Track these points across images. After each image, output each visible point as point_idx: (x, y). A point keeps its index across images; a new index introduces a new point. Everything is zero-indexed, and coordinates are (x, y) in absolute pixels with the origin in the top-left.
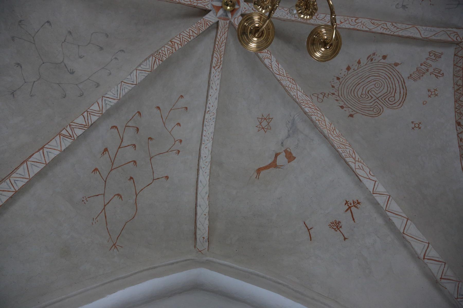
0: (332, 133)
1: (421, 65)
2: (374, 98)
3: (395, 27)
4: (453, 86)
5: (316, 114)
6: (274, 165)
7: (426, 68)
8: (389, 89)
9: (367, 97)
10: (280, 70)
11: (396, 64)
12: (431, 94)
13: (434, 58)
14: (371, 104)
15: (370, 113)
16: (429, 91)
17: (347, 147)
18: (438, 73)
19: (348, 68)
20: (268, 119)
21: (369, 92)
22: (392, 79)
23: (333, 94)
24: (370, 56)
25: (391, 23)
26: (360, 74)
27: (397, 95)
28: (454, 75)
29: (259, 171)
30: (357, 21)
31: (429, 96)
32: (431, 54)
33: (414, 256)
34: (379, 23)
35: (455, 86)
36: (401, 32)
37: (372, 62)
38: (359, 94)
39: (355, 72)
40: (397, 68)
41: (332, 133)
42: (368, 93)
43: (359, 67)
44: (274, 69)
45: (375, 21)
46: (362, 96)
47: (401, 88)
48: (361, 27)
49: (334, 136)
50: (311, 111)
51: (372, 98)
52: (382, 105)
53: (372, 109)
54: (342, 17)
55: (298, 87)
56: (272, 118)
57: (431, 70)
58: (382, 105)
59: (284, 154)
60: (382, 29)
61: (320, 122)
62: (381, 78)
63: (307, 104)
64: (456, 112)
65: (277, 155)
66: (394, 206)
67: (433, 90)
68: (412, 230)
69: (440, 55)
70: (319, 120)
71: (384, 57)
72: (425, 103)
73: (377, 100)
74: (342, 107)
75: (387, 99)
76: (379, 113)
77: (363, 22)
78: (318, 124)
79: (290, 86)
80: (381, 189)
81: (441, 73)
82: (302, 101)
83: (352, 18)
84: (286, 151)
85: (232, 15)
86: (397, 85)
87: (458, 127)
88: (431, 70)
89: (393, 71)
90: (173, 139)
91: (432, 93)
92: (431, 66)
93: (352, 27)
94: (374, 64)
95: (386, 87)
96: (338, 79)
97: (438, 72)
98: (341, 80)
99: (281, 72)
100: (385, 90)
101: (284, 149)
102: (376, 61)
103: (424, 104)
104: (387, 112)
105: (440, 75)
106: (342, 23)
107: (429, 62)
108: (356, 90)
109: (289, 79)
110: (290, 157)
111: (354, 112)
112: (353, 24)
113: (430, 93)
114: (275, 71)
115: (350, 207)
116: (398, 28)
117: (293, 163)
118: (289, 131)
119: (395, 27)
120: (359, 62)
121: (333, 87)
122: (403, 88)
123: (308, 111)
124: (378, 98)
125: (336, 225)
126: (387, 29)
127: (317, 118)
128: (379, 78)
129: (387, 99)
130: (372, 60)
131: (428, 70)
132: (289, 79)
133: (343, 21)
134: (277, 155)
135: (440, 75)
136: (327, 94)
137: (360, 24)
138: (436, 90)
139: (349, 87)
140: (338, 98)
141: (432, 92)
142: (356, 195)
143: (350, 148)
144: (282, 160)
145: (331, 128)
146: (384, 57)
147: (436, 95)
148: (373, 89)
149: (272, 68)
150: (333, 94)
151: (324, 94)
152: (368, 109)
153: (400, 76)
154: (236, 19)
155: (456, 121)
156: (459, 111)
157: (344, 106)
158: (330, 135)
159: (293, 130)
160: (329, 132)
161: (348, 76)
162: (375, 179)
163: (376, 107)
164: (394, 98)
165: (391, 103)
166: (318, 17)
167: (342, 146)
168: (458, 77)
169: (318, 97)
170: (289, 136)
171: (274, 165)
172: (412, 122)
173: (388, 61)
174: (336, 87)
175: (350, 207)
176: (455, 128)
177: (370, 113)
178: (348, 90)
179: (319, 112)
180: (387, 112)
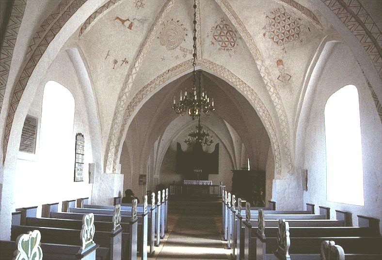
6: (123, 21)
11: (185, 40)
29: (118, 18)
33: (123, 90)
59: (130, 23)
65: (128, 20)
66: (134, 76)
68: (236, 26)
71: (187, 35)
80: (137, 69)
84: (132, 23)
91: (177, 57)
101: (132, 21)
107: (188, 52)
110: (130, 27)
117: (128, 30)
125: (116, 62)
134: (128, 20)
142: (130, 60)
144: (127, 24)
146: (187, 35)
159: (142, 21)
170: (139, 21)
171: (123, 21)
173: (185, 37)
180: (164, 47)
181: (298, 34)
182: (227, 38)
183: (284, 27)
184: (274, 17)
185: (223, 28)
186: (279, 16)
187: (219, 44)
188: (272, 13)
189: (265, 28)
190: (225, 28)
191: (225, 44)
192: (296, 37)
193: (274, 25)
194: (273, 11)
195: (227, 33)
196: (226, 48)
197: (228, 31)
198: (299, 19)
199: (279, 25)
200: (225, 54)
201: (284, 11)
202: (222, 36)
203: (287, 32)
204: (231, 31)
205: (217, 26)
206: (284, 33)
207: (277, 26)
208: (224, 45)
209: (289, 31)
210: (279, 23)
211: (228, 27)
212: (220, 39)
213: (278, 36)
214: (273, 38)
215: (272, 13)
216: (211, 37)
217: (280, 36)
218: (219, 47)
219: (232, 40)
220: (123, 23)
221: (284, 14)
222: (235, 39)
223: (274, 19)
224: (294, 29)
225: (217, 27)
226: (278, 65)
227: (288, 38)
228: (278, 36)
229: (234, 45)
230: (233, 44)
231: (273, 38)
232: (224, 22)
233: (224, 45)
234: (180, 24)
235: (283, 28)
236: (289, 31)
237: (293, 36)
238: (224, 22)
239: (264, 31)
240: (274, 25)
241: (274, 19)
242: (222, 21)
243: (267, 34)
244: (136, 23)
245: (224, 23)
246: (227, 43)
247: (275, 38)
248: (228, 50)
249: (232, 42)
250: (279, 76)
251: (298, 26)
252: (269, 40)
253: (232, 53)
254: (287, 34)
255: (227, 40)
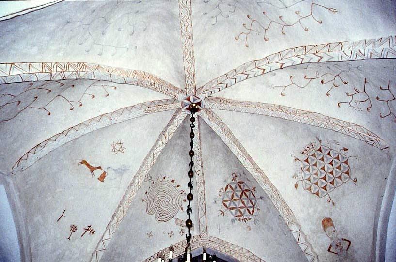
6: (92, 169)
15: (149, 209)
20: (122, 150)
29: (84, 162)
38: (159, 196)
63: (140, 179)
65: (100, 167)
84: (105, 173)
85: (187, 109)
90: (80, 99)
91: (171, 234)
96: (164, 178)
110: (102, 178)
115: (88, 230)
118: (119, 169)
120: (178, 186)
125: (74, 229)
127: (134, 190)
134: (100, 167)
144: (98, 173)
154: (184, 113)
161: (168, 183)
162: (111, 237)
167: (122, 211)
170: (115, 170)
171: (92, 169)
175: (88, 230)
177: (149, 209)
180: (153, 217)
181: (347, 173)
182: (243, 203)
183: (323, 168)
184: (306, 158)
185: (236, 188)
186: (314, 155)
187: (231, 213)
188: (303, 153)
189: (295, 176)
190: (238, 188)
191: (240, 212)
192: (345, 178)
193: (308, 170)
194: (303, 150)
195: (242, 195)
196: (242, 218)
197: (243, 192)
198: (345, 149)
199: (315, 167)
200: (240, 226)
201: (320, 145)
202: (235, 200)
203: (330, 175)
204: (247, 190)
205: (227, 186)
206: (324, 178)
207: (313, 170)
208: (238, 213)
209: (332, 173)
210: (315, 165)
211: (242, 185)
212: (232, 206)
213: (316, 184)
214: (310, 189)
215: (303, 153)
216: (220, 203)
217: (319, 184)
218: (233, 217)
219: (250, 205)
220: (92, 171)
221: (320, 150)
222: (253, 201)
223: (307, 161)
224: (339, 168)
225: (227, 188)
226: (325, 227)
227: (332, 183)
228: (316, 184)
229: (253, 211)
230: (251, 210)
231: (310, 189)
232: (236, 179)
233: (238, 213)
234: (175, 184)
235: (323, 171)
236: (332, 173)
237: (340, 177)
238: (236, 179)
239: (295, 181)
240: (308, 170)
241: (307, 161)
242: (233, 179)
243: (300, 183)
244: (110, 174)
245: (237, 180)
246: (242, 210)
247: (312, 188)
248: (245, 220)
249: (251, 207)
250: (331, 246)
251: (345, 160)
252: (304, 192)
253: (250, 223)
254: (330, 178)
255: (241, 205)
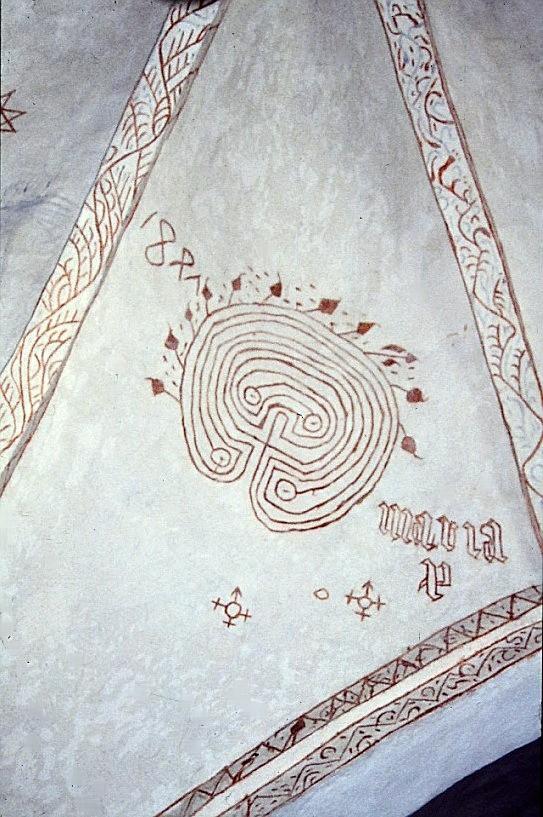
0: (44, 340)
1: (439, 520)
2: (263, 435)
3: (518, 367)
4: (412, 645)
5: (85, 253)
7: (437, 541)
8: (318, 465)
9: (255, 410)
10: (182, 57)
11: (408, 445)
12: (358, 599)
13: (480, 546)
14: (235, 434)
16: (368, 585)
17: (19, 412)
18: (435, 582)
19: (328, 306)
21: (275, 410)
22: (354, 457)
23: (206, 292)
24: (401, 350)
25: (523, 348)
26: (323, 350)
27: (309, 500)
28: (449, 628)
30: (479, 234)
31: (350, 597)
32: (487, 530)
34: (509, 312)
35: (416, 652)
36: (513, 395)
37: (383, 367)
39: (326, 333)
40: (399, 453)
41: (44, 340)
42: (272, 407)
43: (348, 337)
44: (175, 33)
45: (506, 296)
46: (250, 392)
47: (338, 501)
48: (468, 262)
49: (38, 351)
50: (87, 232)
51: (261, 426)
52: (251, 468)
53: (217, 443)
54: (471, 181)
55: (153, 147)
56: (13, 130)
57: (437, 556)
58: (251, 468)
60: (493, 331)
61: (65, 280)
62: (341, 424)
63: (107, 208)
64: (334, 697)
67: (373, 596)
69: (498, 555)
70: (67, 275)
71: (415, 396)
72: (322, 594)
73: (259, 447)
74: (172, 341)
75: (277, 475)
76: (213, 474)
77: (485, 256)
78: (54, 278)
79: (140, 120)
81: (441, 590)
82: (106, 187)
83: (481, 215)
86: (342, 483)
87: (288, 731)
88: (437, 556)
89: (382, 446)
91: (365, 601)
92: (451, 548)
93: (454, 231)
94: (381, 377)
95: (317, 453)
96: (276, 290)
97: (440, 578)
98: (274, 300)
99: (173, 63)
100: (306, 456)
102: (390, 377)
103: (315, 594)
104: (235, 496)
105: (432, 593)
106: (452, 189)
107: (462, 536)
108: (260, 364)
109: (165, 104)
111: (175, 391)
112: (464, 228)
113: (373, 596)
114: (168, 41)
116: (517, 379)
119: (518, 367)
120: (363, 328)
121: (236, 284)
122: (339, 507)
123: (81, 224)
124: (267, 445)
126: (499, 346)
127: (72, 266)
128: (341, 414)
129: (277, 475)
130: (390, 363)
131: (433, 546)
132: (165, 104)
133: (459, 189)
135: (432, 593)
136: (193, 271)
137: (475, 250)
138: (379, 604)
139: (259, 336)
140: (199, 316)
141: (366, 597)
143: (19, 424)
145: (59, 329)
146: (415, 396)
147: (363, 615)
148: (293, 417)
149: (173, 25)
150: (206, 292)
151: (187, 259)
152: (212, 432)
153: (375, 478)
155: (304, 716)
156: (337, 704)
157: (181, 348)
158: (33, 336)
160: (44, 327)
163: (235, 454)
164: (293, 494)
165: (271, 495)
166: (433, 97)
168: (446, 641)
169: (163, 243)
172: (237, 590)
174: (241, 294)
176: (282, 725)
178: (251, 337)
179: (96, 262)
180: (235, 496)
